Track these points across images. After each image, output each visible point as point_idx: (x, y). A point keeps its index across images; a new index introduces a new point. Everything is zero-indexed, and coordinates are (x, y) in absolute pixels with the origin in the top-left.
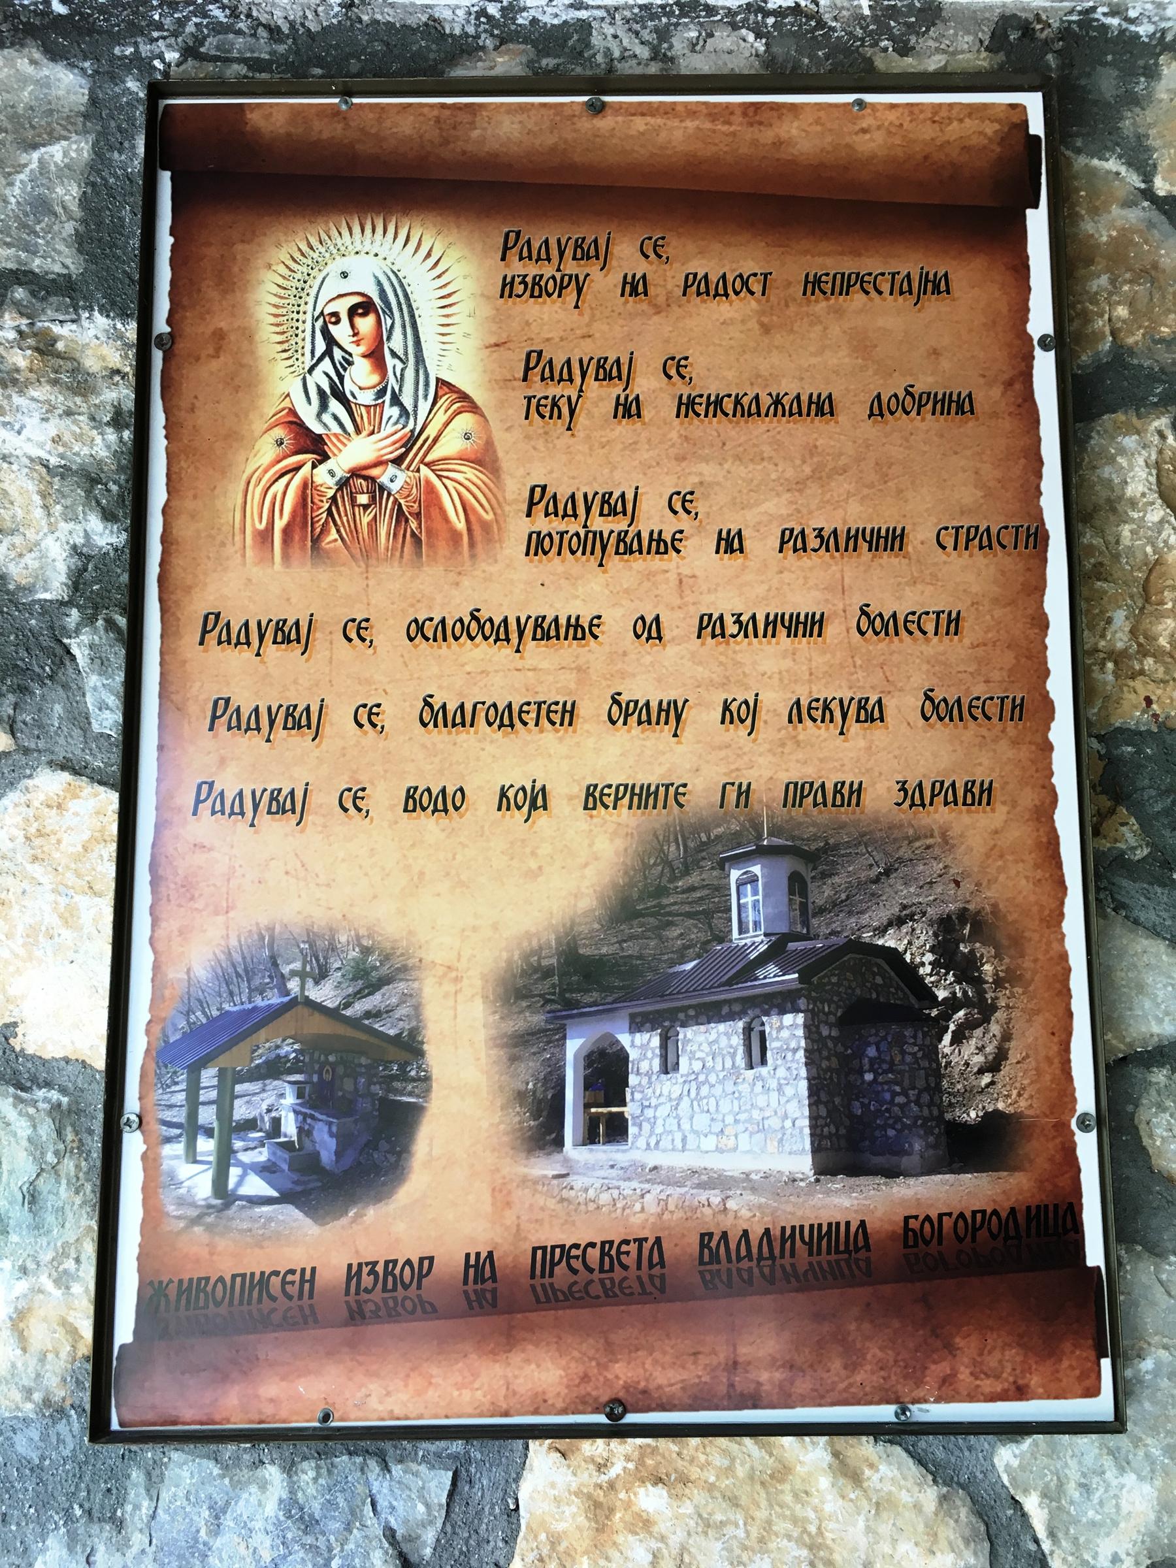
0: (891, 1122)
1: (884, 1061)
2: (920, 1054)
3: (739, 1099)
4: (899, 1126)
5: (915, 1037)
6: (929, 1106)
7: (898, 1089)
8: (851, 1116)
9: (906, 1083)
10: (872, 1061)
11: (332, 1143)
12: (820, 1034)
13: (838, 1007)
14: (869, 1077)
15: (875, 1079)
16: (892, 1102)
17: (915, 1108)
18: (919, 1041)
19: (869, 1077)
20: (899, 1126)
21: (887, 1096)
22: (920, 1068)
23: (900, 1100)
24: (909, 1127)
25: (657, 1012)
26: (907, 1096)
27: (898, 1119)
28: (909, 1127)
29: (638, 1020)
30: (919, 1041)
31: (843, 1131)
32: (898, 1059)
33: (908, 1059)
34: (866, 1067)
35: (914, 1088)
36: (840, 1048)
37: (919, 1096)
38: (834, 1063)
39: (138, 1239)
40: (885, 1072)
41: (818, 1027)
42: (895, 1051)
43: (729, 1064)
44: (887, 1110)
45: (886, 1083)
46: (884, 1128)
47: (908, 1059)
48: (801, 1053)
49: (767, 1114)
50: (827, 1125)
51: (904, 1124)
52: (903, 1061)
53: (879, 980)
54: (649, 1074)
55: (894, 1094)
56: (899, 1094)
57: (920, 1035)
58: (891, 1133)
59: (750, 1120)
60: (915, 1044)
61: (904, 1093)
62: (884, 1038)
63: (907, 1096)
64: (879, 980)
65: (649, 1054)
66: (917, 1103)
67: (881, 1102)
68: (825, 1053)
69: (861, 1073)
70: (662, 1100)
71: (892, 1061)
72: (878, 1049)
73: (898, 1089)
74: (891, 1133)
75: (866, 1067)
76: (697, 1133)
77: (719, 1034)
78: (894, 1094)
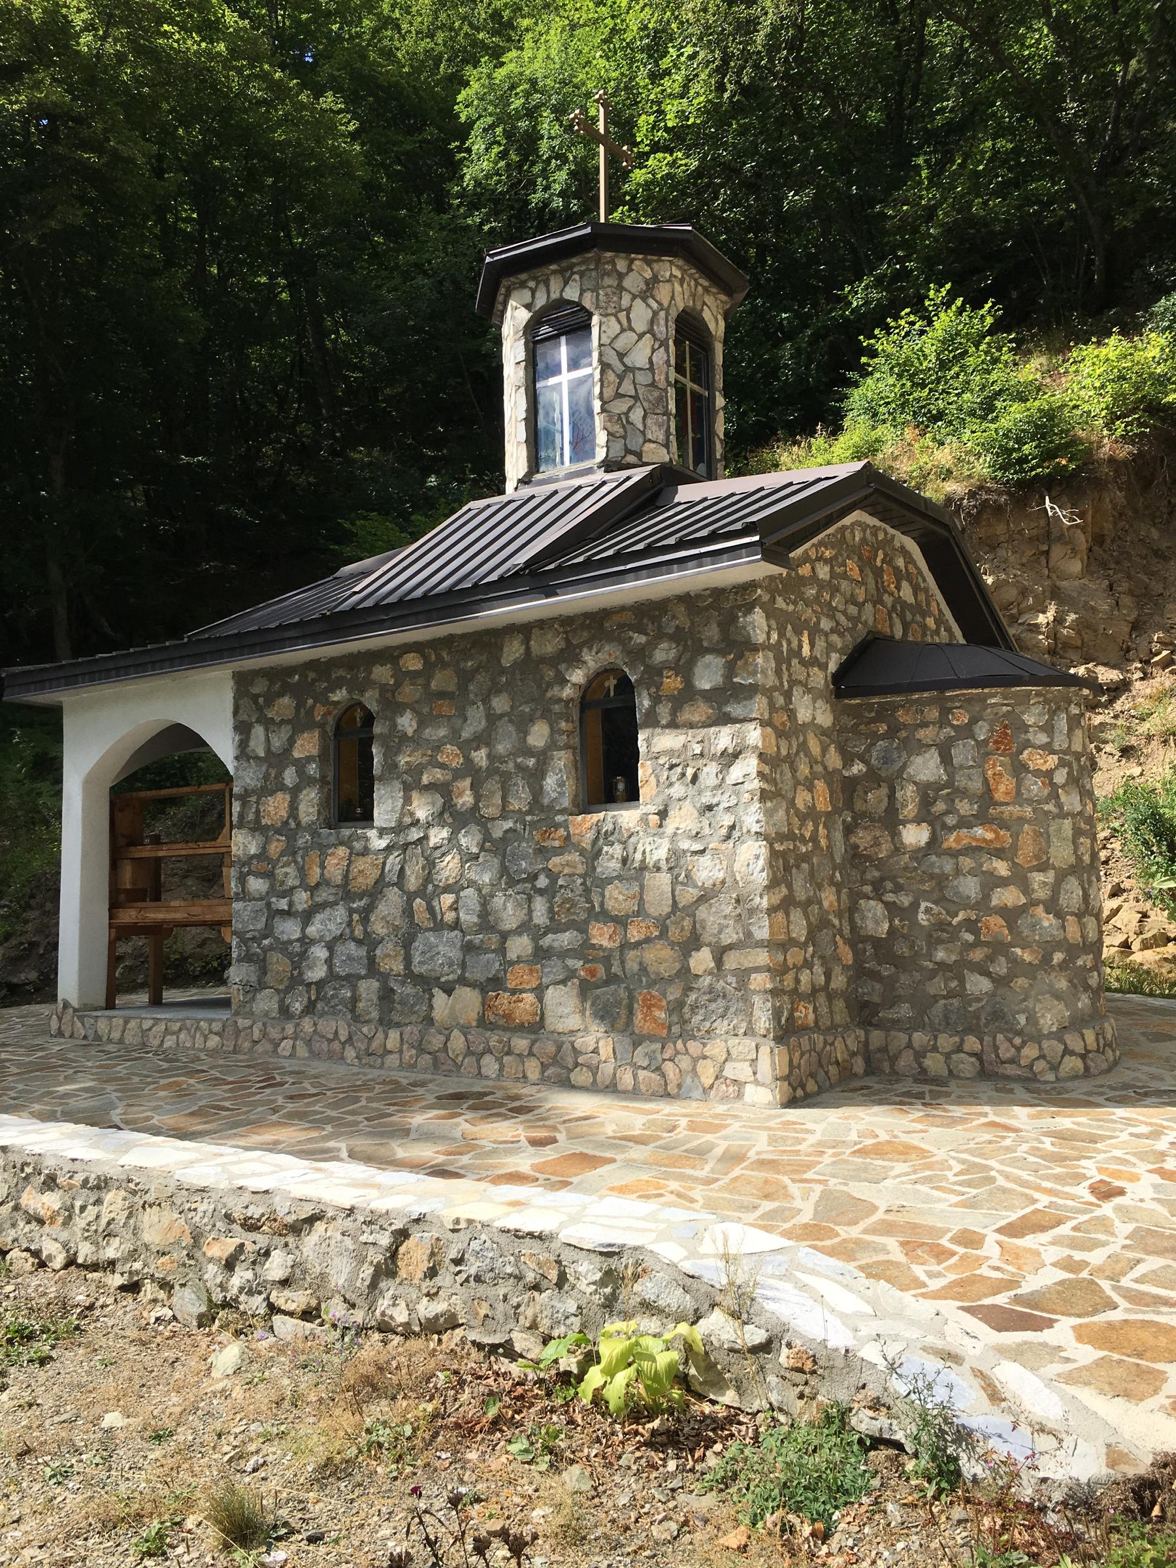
0: (977, 955)
1: (964, 793)
2: (1060, 777)
3: (548, 893)
4: (1001, 967)
5: (1049, 728)
6: (1079, 916)
7: (1002, 868)
8: (857, 939)
9: (1027, 849)
10: (927, 794)
11: (1116, 672)
12: (792, 715)
13: (830, 648)
14: (915, 835)
15: (934, 842)
16: (983, 904)
17: (1048, 921)
18: (1060, 742)
19: (915, 835)
20: (1001, 967)
21: (970, 887)
22: (1063, 815)
23: (1009, 897)
24: (1030, 971)
25: (313, 664)
26: (1025, 888)
27: (999, 948)
28: (1030, 971)
29: (259, 687)
30: (1060, 742)
31: (839, 981)
32: (1004, 788)
33: (1035, 787)
34: (910, 809)
35: (1043, 868)
36: (834, 760)
37: (1056, 888)
38: (822, 798)
39: (459, 632)
40: (965, 823)
41: (788, 695)
42: (997, 766)
43: (520, 800)
44: (971, 926)
45: (969, 851)
46: (956, 970)
47: (1035, 787)
48: (748, 766)
49: (635, 934)
50: (808, 964)
51: (1014, 961)
52: (1018, 797)
53: (906, 593)
54: (289, 828)
55: (992, 882)
56: (1003, 882)
57: (1062, 723)
58: (979, 984)
59: (585, 950)
60: (1048, 748)
61: (1019, 879)
62: (966, 731)
63: (1025, 888)
64: (906, 593)
65: (290, 776)
66: (1052, 906)
67: (951, 903)
68: (804, 769)
69: (891, 821)
70: (324, 895)
71: (988, 793)
72: (946, 759)
73: (1002, 868)
74: (979, 984)
75: (910, 809)
76: (427, 983)
77: (492, 719)
78: (992, 882)
